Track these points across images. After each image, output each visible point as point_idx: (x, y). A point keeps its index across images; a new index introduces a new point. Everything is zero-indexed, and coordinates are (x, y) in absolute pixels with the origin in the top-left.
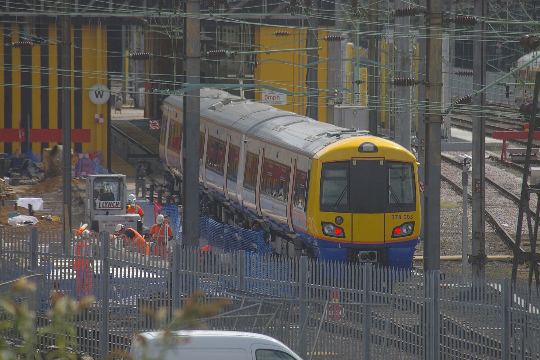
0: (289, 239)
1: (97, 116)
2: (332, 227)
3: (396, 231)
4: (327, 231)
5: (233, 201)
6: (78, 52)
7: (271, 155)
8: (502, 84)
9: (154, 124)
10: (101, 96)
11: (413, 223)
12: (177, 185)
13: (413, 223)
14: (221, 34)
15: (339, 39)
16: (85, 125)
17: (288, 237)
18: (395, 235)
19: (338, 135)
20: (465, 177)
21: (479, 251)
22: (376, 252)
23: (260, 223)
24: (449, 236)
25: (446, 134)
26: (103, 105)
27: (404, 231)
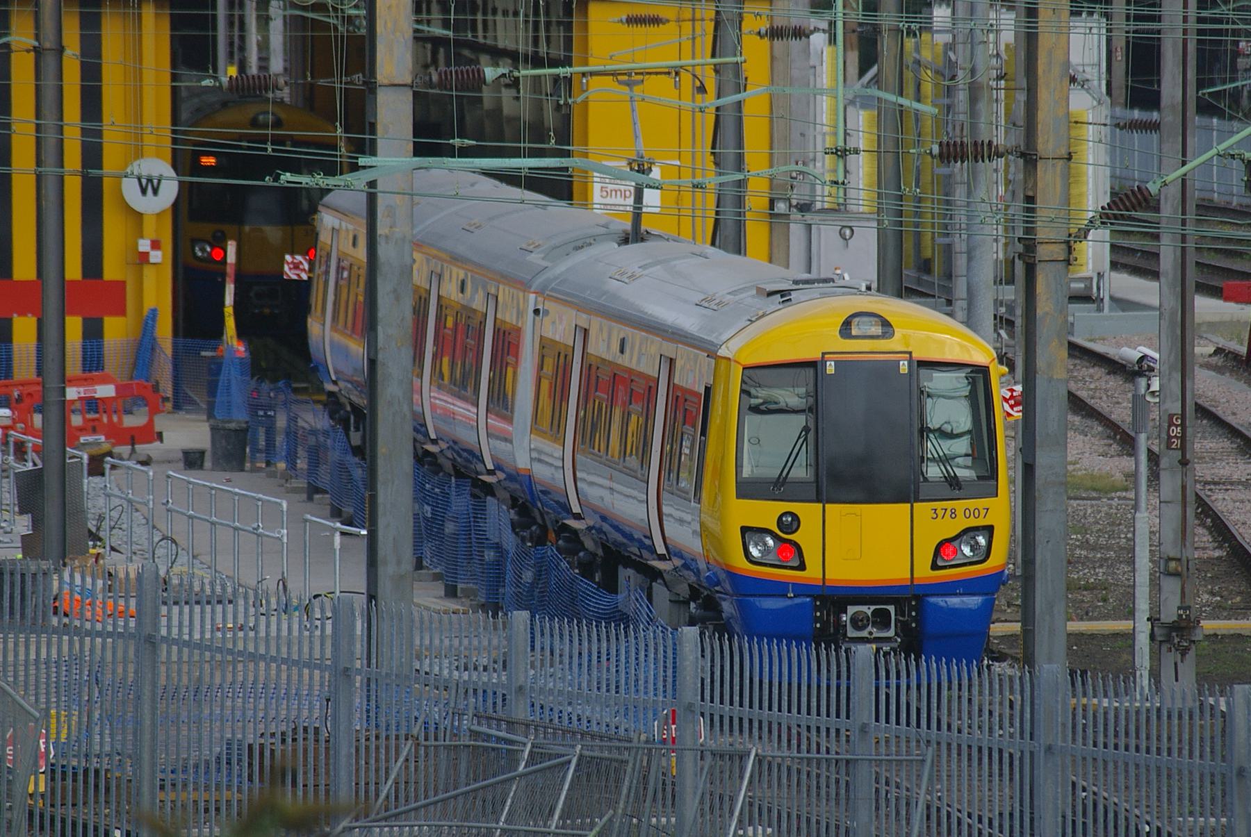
0: (655, 574)
1: (144, 245)
2: (770, 542)
4: (755, 552)
5: (681, 557)
6: (91, 73)
7: (603, 346)
8: (1233, 156)
9: (296, 266)
10: (155, 192)
11: (989, 530)
12: (357, 429)
13: (989, 530)
14: (485, 22)
15: (800, 33)
16: (112, 270)
17: (653, 569)
18: (940, 563)
19: (783, 293)
20: (1138, 404)
21: (1179, 608)
22: (891, 608)
23: (575, 532)
24: (1101, 566)
25: (1099, 289)
26: (159, 215)
27: (967, 550)
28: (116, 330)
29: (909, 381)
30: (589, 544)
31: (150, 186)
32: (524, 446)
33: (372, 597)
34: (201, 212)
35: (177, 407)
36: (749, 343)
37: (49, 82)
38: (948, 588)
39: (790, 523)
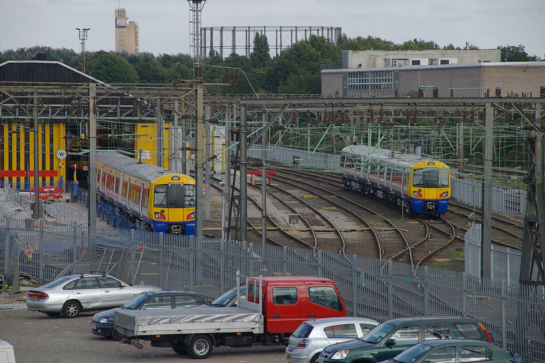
1: (61, 165)
3: (189, 216)
6: (51, 136)
28: (55, 179)
29: (182, 188)
30: (131, 215)
31: (61, 154)
32: (119, 198)
33: (89, 225)
34: (70, 159)
35: (66, 192)
36: (156, 181)
37: (36, 137)
38: (189, 222)
39: (163, 212)
